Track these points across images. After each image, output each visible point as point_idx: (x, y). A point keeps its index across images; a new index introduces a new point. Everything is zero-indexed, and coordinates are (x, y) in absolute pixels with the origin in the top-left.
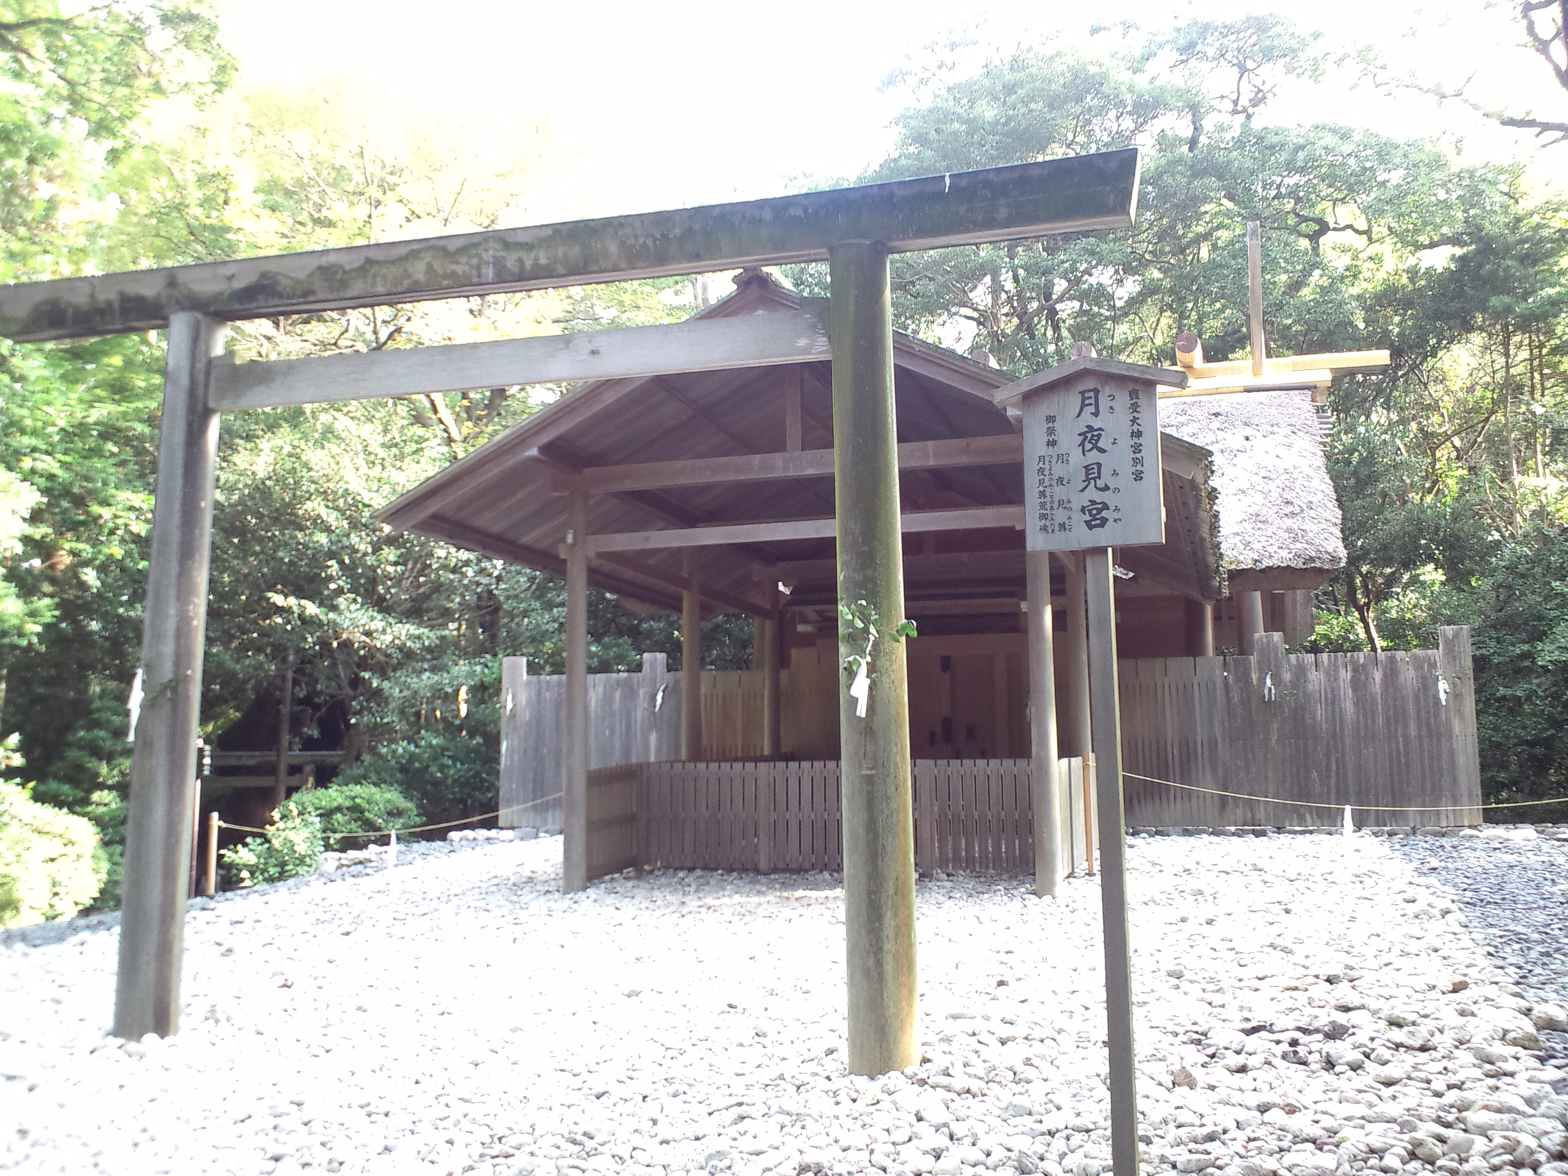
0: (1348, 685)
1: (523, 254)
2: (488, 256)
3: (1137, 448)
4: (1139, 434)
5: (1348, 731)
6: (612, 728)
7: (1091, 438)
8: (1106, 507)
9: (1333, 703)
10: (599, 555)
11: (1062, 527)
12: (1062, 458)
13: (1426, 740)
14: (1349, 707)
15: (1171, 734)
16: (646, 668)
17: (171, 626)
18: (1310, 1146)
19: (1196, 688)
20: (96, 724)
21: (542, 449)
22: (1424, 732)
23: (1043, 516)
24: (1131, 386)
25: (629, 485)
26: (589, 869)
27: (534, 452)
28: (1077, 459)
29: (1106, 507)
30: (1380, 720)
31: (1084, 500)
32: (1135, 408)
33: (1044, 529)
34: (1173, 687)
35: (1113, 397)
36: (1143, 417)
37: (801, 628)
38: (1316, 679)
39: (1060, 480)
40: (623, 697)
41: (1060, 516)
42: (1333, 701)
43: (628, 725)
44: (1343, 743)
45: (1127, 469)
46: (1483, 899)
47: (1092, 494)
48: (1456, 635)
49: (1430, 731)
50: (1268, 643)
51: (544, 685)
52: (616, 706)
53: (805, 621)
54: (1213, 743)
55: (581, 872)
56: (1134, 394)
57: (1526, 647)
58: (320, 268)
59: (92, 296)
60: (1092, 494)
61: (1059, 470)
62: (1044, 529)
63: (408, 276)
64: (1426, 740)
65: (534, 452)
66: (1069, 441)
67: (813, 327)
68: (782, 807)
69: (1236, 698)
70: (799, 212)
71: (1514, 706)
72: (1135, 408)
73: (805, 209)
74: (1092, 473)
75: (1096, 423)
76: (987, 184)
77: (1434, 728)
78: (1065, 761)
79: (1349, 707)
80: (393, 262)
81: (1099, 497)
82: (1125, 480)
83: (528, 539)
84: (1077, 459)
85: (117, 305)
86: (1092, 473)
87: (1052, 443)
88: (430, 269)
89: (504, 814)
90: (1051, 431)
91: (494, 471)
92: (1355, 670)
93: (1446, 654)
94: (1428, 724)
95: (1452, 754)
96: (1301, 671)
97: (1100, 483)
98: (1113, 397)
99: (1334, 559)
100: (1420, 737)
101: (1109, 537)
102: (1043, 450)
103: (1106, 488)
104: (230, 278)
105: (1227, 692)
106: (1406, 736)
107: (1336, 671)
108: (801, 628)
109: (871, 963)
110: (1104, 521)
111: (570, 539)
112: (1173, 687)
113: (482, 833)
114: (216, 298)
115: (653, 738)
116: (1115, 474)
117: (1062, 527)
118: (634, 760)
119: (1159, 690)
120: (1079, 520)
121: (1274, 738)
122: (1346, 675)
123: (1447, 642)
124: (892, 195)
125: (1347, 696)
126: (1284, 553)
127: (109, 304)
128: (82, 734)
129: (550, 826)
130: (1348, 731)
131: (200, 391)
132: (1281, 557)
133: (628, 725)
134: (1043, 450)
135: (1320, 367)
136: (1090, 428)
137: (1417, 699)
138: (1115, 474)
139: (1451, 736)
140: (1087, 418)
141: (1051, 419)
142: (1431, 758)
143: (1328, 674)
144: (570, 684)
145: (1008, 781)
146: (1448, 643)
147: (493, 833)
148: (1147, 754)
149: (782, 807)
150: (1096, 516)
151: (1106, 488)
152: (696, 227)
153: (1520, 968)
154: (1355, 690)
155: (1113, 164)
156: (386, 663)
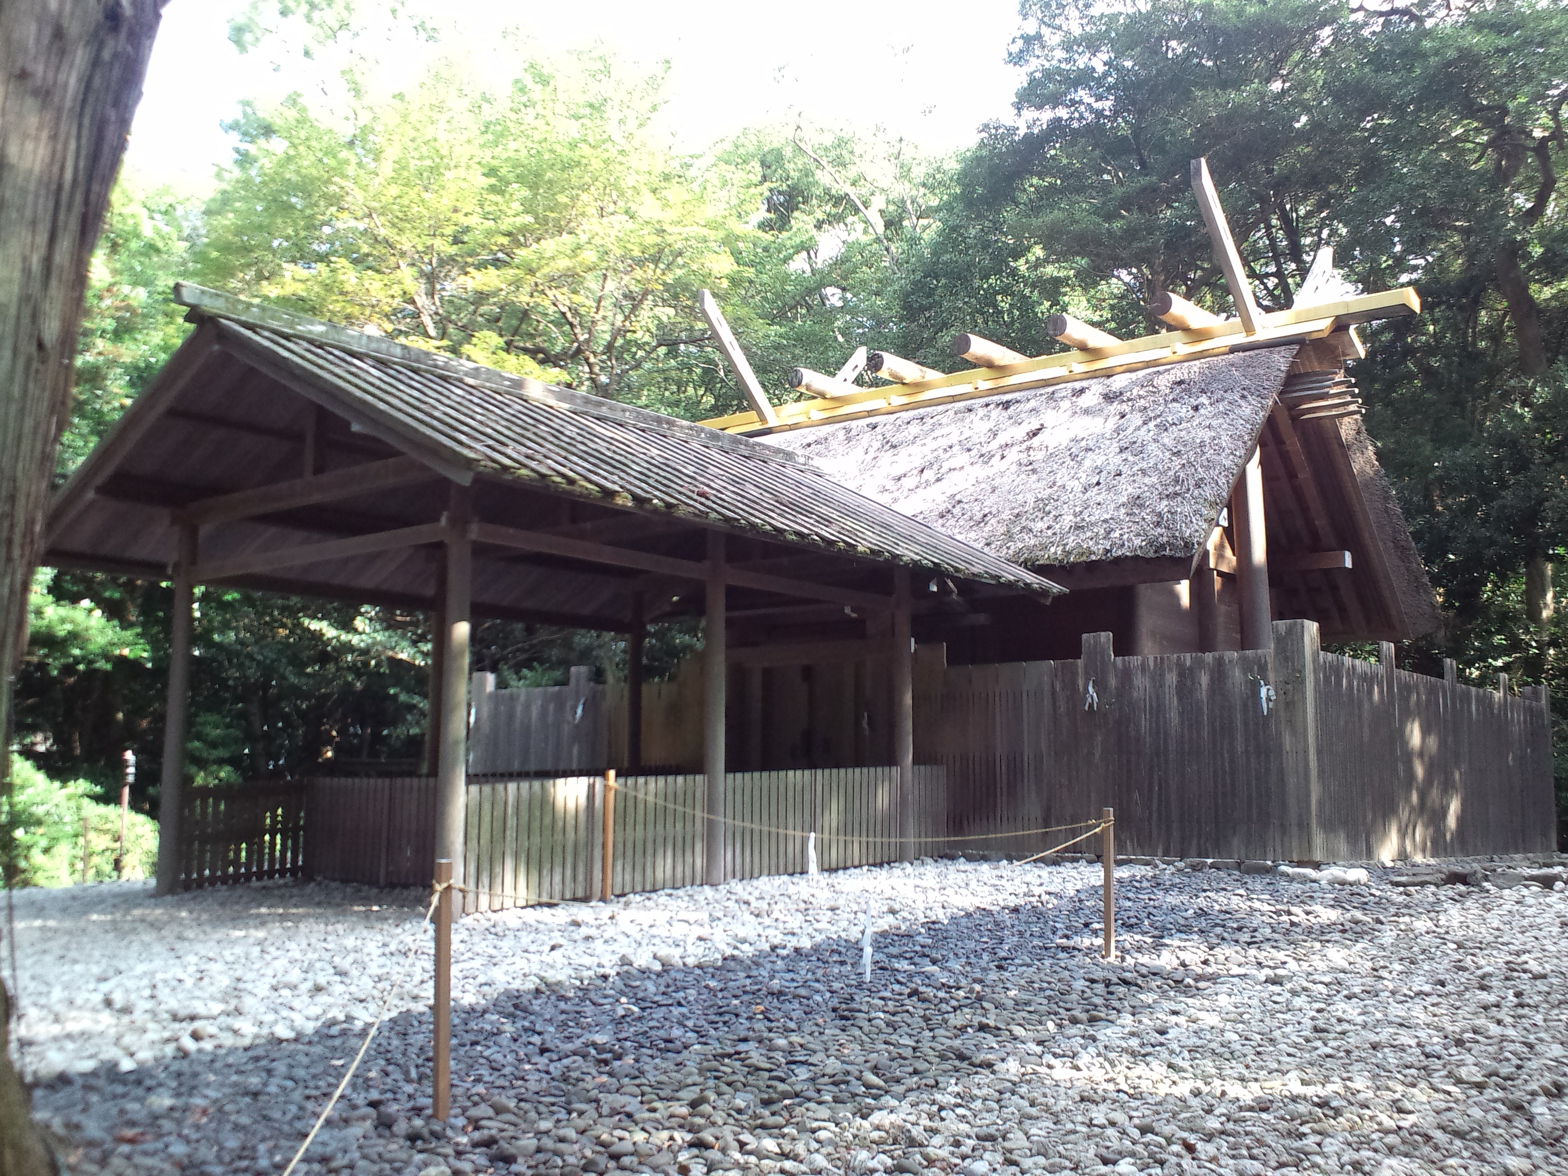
0: (1173, 691)
22: (1251, 749)
42: (1158, 711)
92: (1181, 675)
107: (1162, 675)
143: (1153, 678)
154: (1180, 700)
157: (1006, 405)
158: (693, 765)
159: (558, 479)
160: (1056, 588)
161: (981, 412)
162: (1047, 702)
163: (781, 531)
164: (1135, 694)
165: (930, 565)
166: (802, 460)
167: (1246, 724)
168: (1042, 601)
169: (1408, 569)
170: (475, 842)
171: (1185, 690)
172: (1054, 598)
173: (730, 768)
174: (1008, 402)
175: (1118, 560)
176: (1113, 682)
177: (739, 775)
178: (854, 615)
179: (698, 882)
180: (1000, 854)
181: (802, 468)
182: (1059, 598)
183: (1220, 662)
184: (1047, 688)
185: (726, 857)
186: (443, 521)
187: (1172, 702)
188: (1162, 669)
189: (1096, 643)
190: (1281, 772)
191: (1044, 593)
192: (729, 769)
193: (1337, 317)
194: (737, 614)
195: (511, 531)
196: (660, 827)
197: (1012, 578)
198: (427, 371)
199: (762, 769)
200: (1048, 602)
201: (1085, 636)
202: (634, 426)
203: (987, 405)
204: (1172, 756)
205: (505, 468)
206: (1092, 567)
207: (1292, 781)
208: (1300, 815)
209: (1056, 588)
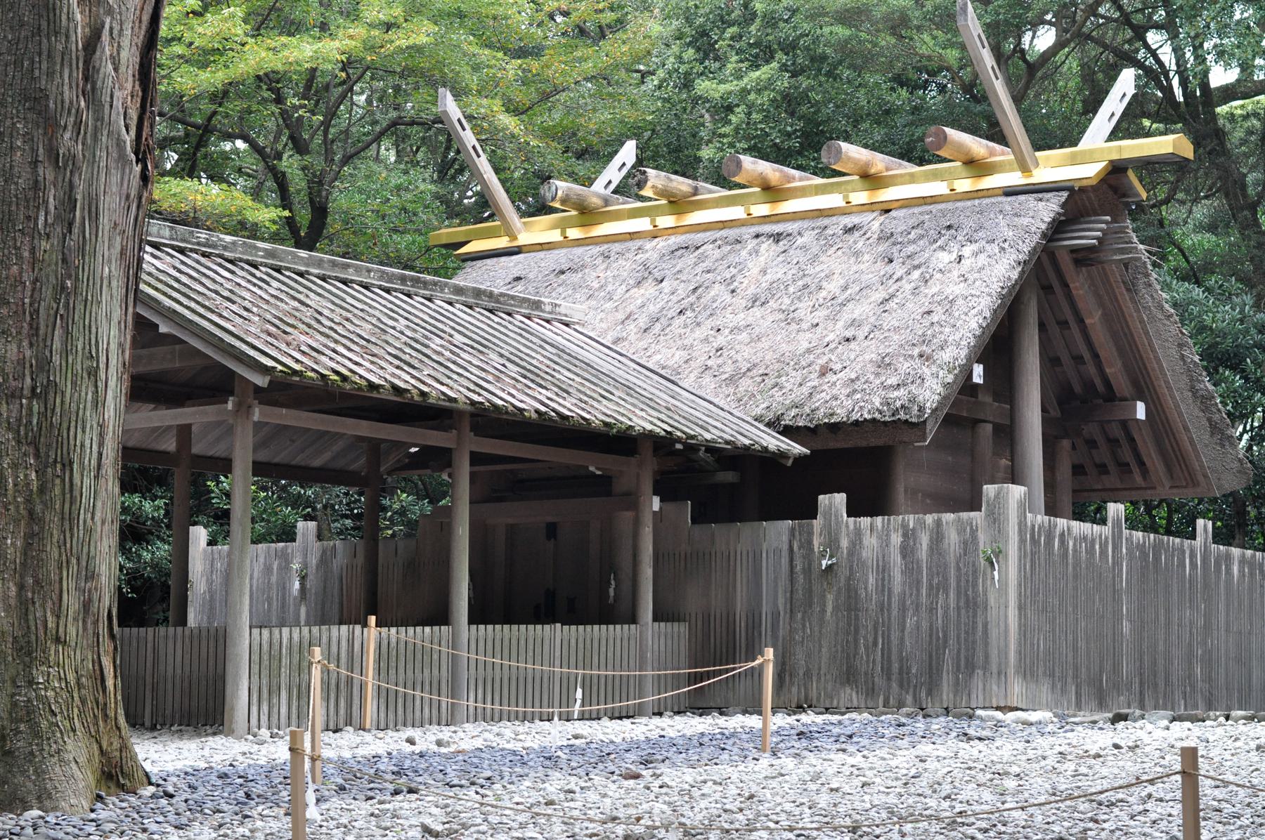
0: (897, 551)
6: (269, 600)
9: (884, 571)
13: (963, 611)
15: (740, 607)
17: (65, 10)
19: (764, 555)
22: (962, 604)
34: (744, 553)
42: (883, 569)
43: (283, 606)
44: (889, 614)
49: (967, 601)
50: (830, 503)
51: (216, 556)
52: (274, 579)
54: (776, 616)
64: (963, 611)
78: (656, 624)
92: (905, 535)
93: (987, 516)
94: (966, 595)
100: (958, 608)
105: (791, 560)
106: (946, 609)
107: (888, 535)
112: (744, 553)
115: (303, 610)
119: (732, 559)
121: (829, 609)
122: (896, 539)
139: (986, 608)
142: (967, 633)
143: (879, 537)
148: (718, 630)
154: (904, 557)
157: (777, 237)
158: (439, 615)
159: (336, 378)
160: (798, 449)
161: (752, 244)
162: (785, 561)
163: (521, 410)
164: (864, 554)
165: (663, 433)
166: (548, 308)
167: (959, 581)
168: (783, 461)
169: (1209, 420)
170: (257, 677)
171: (907, 551)
172: (795, 459)
173: (476, 617)
174: (779, 234)
175: (856, 423)
176: (844, 543)
177: (482, 627)
178: (599, 473)
179: (444, 722)
180: (738, 709)
181: (548, 316)
182: (799, 459)
183: (938, 523)
184: (785, 547)
185: (468, 702)
186: (230, 406)
187: (896, 559)
188: (888, 531)
189: (830, 503)
190: (985, 625)
191: (782, 455)
192: (472, 621)
193: (1111, 162)
194: (482, 468)
195: (284, 411)
196: (410, 673)
197: (747, 442)
198: (192, 250)
199: (503, 623)
200: (790, 463)
201: (821, 497)
202: (380, 287)
203: (757, 236)
204: (895, 613)
205: (295, 372)
206: (835, 428)
207: (994, 633)
208: (1000, 664)
209: (798, 449)
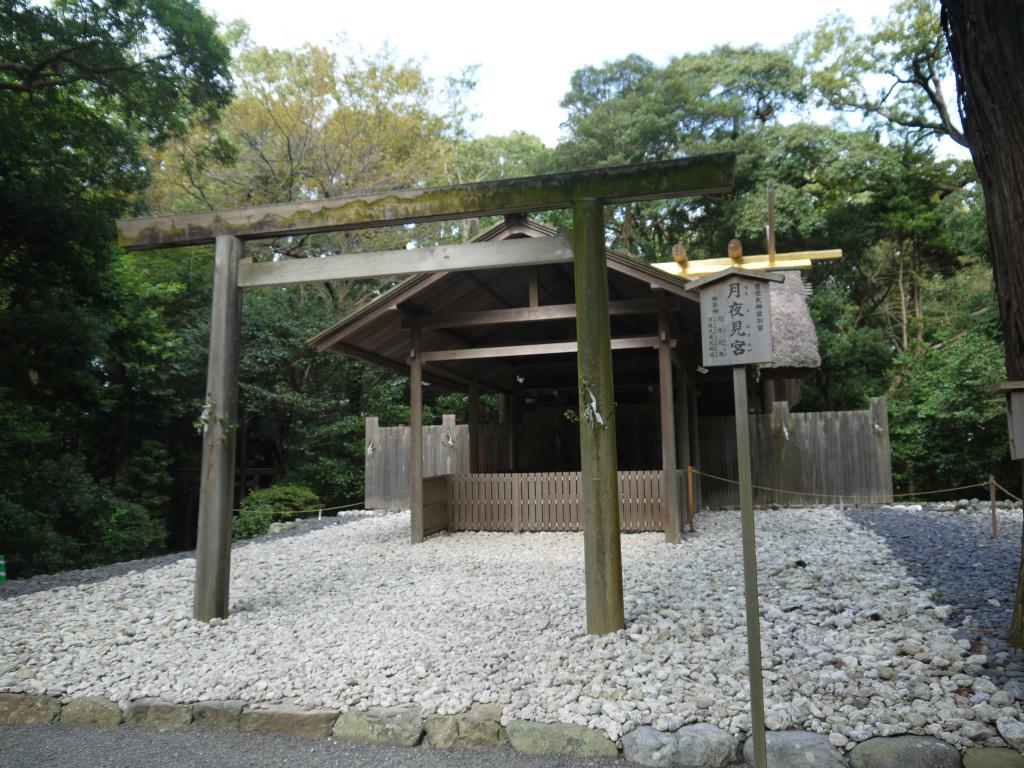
1: (407, 205)
2: (388, 206)
3: (759, 314)
4: (760, 307)
5: (822, 455)
7: (736, 308)
8: (744, 344)
10: (428, 363)
11: (721, 354)
12: (721, 319)
14: (822, 442)
16: (444, 422)
18: (832, 666)
20: (145, 454)
21: (398, 306)
23: (711, 349)
24: (755, 283)
25: (444, 325)
26: (425, 530)
27: (394, 307)
28: (729, 319)
29: (744, 344)
30: (839, 448)
31: (733, 340)
32: (758, 293)
33: (712, 355)
35: (746, 288)
36: (763, 297)
37: (528, 401)
38: (805, 426)
39: (720, 330)
40: (432, 438)
41: (720, 348)
42: (814, 439)
43: (435, 457)
45: (754, 324)
46: (904, 544)
47: (736, 337)
48: (879, 402)
53: (530, 397)
55: (421, 532)
56: (757, 286)
57: (912, 407)
58: (299, 212)
59: (173, 226)
60: (736, 337)
61: (719, 325)
62: (712, 355)
63: (345, 216)
65: (394, 307)
66: (724, 310)
67: (564, 244)
68: (525, 497)
69: (763, 436)
70: (556, 183)
71: (908, 439)
72: (758, 293)
73: (559, 181)
74: (736, 326)
75: (738, 301)
76: (656, 169)
77: (868, 455)
79: (822, 442)
80: (337, 209)
81: (740, 339)
82: (753, 330)
83: (386, 354)
84: (729, 319)
85: (187, 232)
86: (736, 326)
87: (716, 311)
88: (357, 213)
89: (368, 503)
90: (715, 305)
91: (372, 317)
92: (826, 421)
95: (877, 465)
96: (798, 421)
97: (741, 332)
98: (746, 288)
99: (815, 362)
101: (744, 359)
102: (711, 315)
103: (744, 334)
104: (249, 217)
108: (528, 401)
109: (599, 577)
110: (743, 351)
111: (412, 355)
113: (356, 512)
114: (242, 227)
115: (449, 460)
116: (748, 327)
117: (721, 354)
118: (439, 474)
120: (730, 351)
123: (874, 406)
124: (605, 174)
125: (821, 434)
126: (788, 359)
127: (183, 231)
128: (138, 459)
129: (393, 508)
130: (822, 455)
131: (234, 278)
132: (786, 361)
133: (435, 457)
134: (711, 315)
135: (804, 259)
136: (735, 304)
137: (858, 437)
138: (748, 327)
140: (734, 298)
141: (715, 299)
144: (412, 433)
145: (648, 483)
146: (874, 406)
147: (362, 512)
149: (525, 497)
150: (739, 351)
151: (744, 334)
152: (501, 191)
153: (897, 587)
155: (723, 159)
156: (310, 419)
